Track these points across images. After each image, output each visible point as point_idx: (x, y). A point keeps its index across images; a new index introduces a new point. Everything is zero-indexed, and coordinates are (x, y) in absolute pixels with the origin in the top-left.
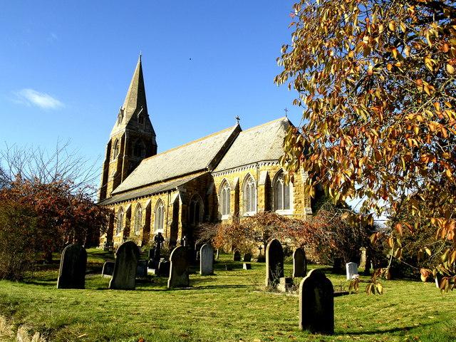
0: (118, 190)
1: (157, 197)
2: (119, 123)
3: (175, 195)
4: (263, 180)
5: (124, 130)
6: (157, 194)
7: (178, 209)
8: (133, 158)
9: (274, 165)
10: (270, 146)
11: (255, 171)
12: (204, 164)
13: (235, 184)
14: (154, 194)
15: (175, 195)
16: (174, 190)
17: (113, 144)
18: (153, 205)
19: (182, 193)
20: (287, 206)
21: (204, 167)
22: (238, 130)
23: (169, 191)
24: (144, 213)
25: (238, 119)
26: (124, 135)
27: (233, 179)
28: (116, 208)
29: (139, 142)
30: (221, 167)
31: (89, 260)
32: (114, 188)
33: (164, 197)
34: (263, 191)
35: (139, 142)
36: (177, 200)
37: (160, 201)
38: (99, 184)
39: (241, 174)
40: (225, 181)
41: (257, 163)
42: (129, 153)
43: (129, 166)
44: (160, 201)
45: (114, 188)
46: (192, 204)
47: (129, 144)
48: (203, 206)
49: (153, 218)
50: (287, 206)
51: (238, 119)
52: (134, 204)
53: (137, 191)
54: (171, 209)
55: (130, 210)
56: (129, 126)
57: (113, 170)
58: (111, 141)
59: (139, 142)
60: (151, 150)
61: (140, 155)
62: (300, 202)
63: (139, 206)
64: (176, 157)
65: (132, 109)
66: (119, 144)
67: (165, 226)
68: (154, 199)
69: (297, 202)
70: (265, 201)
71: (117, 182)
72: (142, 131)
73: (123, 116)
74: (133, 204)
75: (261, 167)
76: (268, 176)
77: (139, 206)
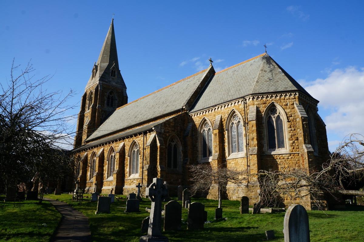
0: (93, 136)
1: (131, 140)
2: (93, 77)
3: (151, 136)
4: (252, 114)
5: (98, 82)
6: (131, 136)
7: (99, 167)
8: (106, 108)
9: (264, 99)
10: (256, 80)
11: (242, 106)
12: (180, 103)
13: (218, 123)
14: (128, 137)
15: (151, 136)
16: (150, 131)
17: (87, 96)
18: (127, 148)
19: (159, 134)
20: (281, 145)
21: (180, 107)
22: (211, 73)
23: (145, 133)
24: (117, 156)
25: (211, 61)
26: (97, 87)
27: (214, 117)
28: (89, 153)
29: (110, 93)
30: (198, 106)
31: (140, 208)
32: (88, 137)
33: (139, 140)
34: (255, 128)
35: (111, 93)
36: (154, 141)
37: (134, 144)
38: (54, 144)
39: (224, 111)
40: (205, 120)
41: (243, 97)
42: (102, 103)
43: (101, 115)
44: (134, 144)
45: (88, 137)
46: (170, 144)
47: (102, 95)
48: (181, 148)
49: (127, 162)
50: (281, 145)
51: (211, 61)
52: (107, 148)
53: (110, 137)
54: (148, 151)
55: (103, 153)
56: (102, 79)
57: (87, 120)
58: (86, 94)
59: (110, 93)
60: (123, 101)
61: (112, 106)
62: (297, 139)
63: (112, 150)
64: (150, 99)
65: (106, 65)
66: (93, 96)
67: (140, 170)
68: (128, 143)
69: (294, 138)
70: (257, 139)
71: (93, 127)
72: (114, 84)
73: (97, 71)
74: (106, 149)
75: (249, 101)
76: (258, 111)
77: (112, 150)
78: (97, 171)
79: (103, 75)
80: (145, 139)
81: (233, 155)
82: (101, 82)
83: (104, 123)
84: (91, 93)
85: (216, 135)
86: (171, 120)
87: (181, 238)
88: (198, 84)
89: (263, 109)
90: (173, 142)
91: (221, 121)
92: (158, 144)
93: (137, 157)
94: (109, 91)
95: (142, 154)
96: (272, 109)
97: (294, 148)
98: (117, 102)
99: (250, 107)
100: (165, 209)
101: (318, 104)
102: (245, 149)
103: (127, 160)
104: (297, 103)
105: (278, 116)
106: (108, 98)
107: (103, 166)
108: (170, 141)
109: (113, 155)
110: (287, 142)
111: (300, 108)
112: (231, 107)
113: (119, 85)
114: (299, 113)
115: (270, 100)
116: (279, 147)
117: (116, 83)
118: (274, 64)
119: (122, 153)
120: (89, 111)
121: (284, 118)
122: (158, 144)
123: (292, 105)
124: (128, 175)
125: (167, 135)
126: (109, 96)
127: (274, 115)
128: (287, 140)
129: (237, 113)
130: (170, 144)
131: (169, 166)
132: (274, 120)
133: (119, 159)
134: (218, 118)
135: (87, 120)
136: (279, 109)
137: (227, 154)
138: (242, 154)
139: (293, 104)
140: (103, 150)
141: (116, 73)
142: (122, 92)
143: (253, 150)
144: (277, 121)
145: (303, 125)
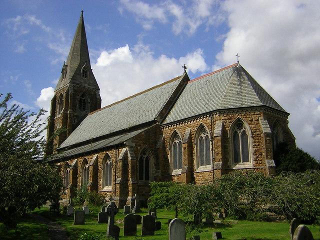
4: (218, 130)
16: (121, 145)
24: (91, 169)
34: (220, 143)
35: (83, 96)
36: (126, 154)
43: (72, 123)
48: (152, 161)
50: (246, 159)
54: (120, 164)
56: (73, 80)
69: (257, 153)
78: (71, 183)
79: (73, 76)
80: (117, 152)
81: (201, 169)
82: (72, 85)
83: (76, 129)
84: (62, 95)
85: (185, 148)
86: (143, 133)
87: (65, 188)
88: (171, 92)
89: (229, 124)
90: (145, 154)
91: (190, 135)
92: (130, 159)
93: (111, 170)
94: (81, 94)
95: (114, 167)
96: (239, 124)
97: (257, 163)
98: (89, 105)
99: (217, 122)
100: (142, 222)
101: (289, 119)
102: (212, 162)
103: (100, 173)
104: (262, 118)
105: (244, 131)
106: (80, 101)
107: (77, 178)
108: (141, 154)
109: (87, 166)
110: (251, 157)
111: (265, 123)
112: (200, 121)
113: (92, 87)
114: (265, 127)
115: (237, 116)
116: (243, 161)
117: (89, 85)
118: (245, 77)
119: (96, 165)
120: (60, 116)
121: (249, 133)
122: (130, 159)
123: (256, 120)
124: (102, 187)
125: (139, 148)
126: (81, 99)
127: (240, 130)
128: (251, 155)
129: (206, 127)
130: (141, 157)
131: (141, 178)
132: (240, 134)
133: (93, 171)
134: (188, 131)
135: (58, 126)
136: (246, 125)
137: (195, 168)
138: (209, 168)
139: (258, 120)
140: (77, 161)
141: (88, 73)
142: (95, 94)
143: (217, 165)
144: (242, 136)
145: (266, 140)
